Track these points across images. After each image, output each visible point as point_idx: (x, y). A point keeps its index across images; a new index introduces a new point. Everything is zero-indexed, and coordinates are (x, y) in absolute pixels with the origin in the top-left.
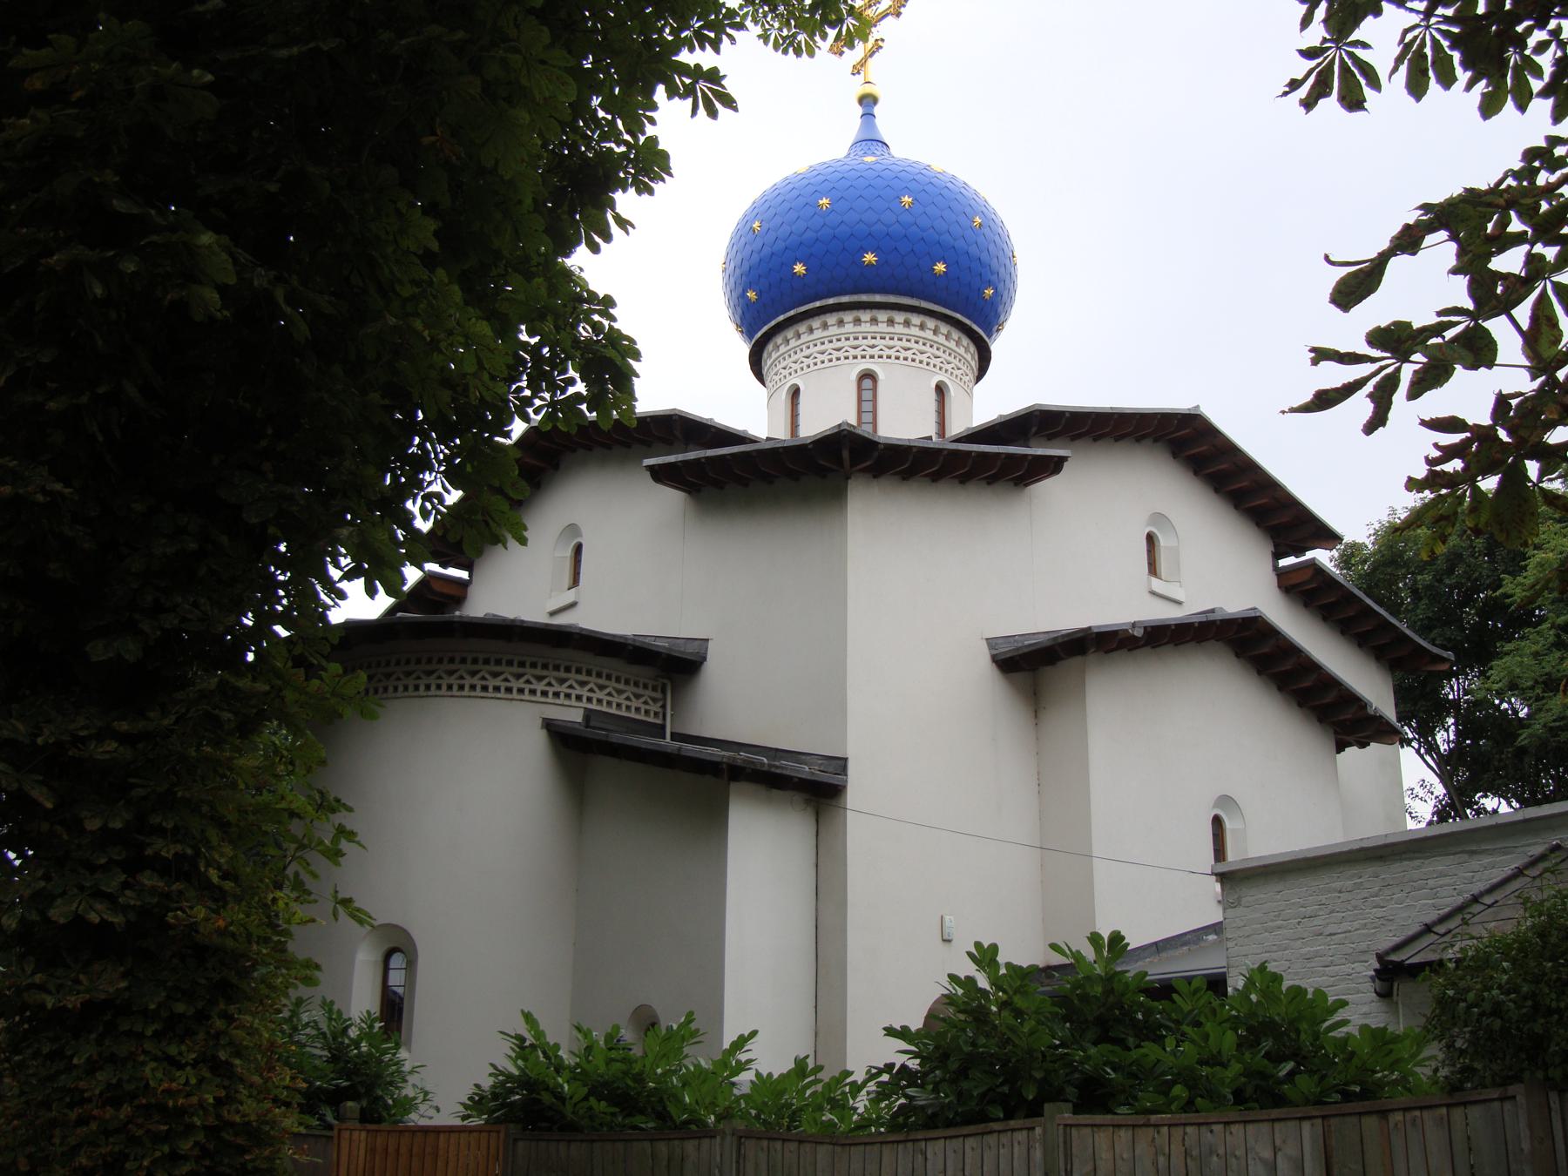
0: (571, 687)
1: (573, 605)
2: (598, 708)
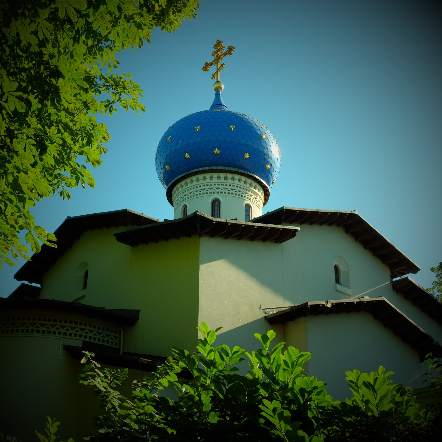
0: (77, 331)
1: (83, 297)
2: (89, 340)
